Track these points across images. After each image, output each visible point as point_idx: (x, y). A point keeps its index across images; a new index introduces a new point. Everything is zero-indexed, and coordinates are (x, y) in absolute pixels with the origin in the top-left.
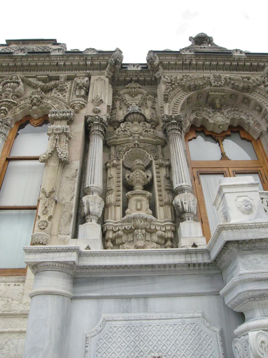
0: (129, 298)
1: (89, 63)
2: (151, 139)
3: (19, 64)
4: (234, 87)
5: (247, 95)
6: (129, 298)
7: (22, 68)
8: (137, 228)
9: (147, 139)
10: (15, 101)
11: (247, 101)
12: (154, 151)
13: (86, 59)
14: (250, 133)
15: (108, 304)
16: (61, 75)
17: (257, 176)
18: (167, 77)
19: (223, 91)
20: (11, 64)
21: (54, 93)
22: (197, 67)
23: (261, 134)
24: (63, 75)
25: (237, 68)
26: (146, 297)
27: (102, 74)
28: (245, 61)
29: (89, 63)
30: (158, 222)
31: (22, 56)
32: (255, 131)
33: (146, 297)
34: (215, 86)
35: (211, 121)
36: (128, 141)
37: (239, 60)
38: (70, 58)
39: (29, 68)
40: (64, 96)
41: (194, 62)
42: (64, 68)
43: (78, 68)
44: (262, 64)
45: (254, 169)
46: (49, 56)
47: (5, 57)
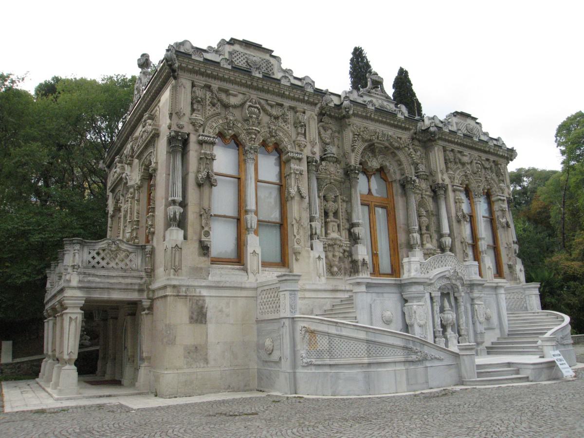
0: (378, 293)
1: (306, 98)
2: (339, 179)
3: (255, 84)
4: (391, 144)
5: (396, 151)
6: (378, 293)
7: (257, 89)
8: (335, 244)
9: (337, 178)
10: (257, 129)
11: (394, 155)
12: (340, 189)
13: (305, 94)
14: (387, 175)
15: (374, 295)
16: (284, 104)
17: (385, 210)
18: (568, 392)
19: (383, 144)
20: (249, 83)
21: (281, 123)
22: (372, 120)
23: (395, 181)
24: (287, 103)
25: (396, 126)
26: (383, 293)
27: (313, 111)
28: (403, 122)
29: (306, 98)
30: (375, 255)
31: (259, 78)
32: (391, 177)
33: (383, 293)
34: (381, 140)
35: (369, 164)
36: (327, 178)
37: (399, 121)
38: (294, 91)
39: (262, 90)
40: (288, 128)
41: (373, 116)
42: (288, 97)
43: (298, 100)
44: (411, 127)
45: (385, 205)
46: (279, 84)
47: (245, 75)
